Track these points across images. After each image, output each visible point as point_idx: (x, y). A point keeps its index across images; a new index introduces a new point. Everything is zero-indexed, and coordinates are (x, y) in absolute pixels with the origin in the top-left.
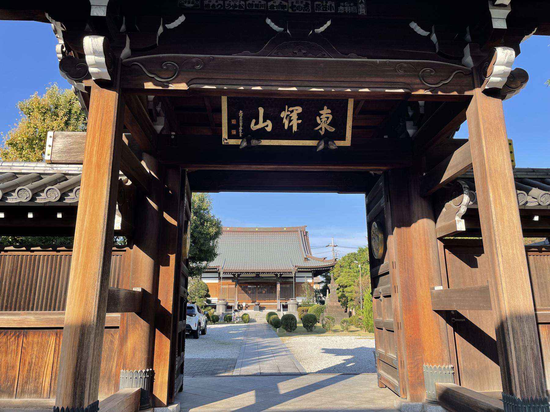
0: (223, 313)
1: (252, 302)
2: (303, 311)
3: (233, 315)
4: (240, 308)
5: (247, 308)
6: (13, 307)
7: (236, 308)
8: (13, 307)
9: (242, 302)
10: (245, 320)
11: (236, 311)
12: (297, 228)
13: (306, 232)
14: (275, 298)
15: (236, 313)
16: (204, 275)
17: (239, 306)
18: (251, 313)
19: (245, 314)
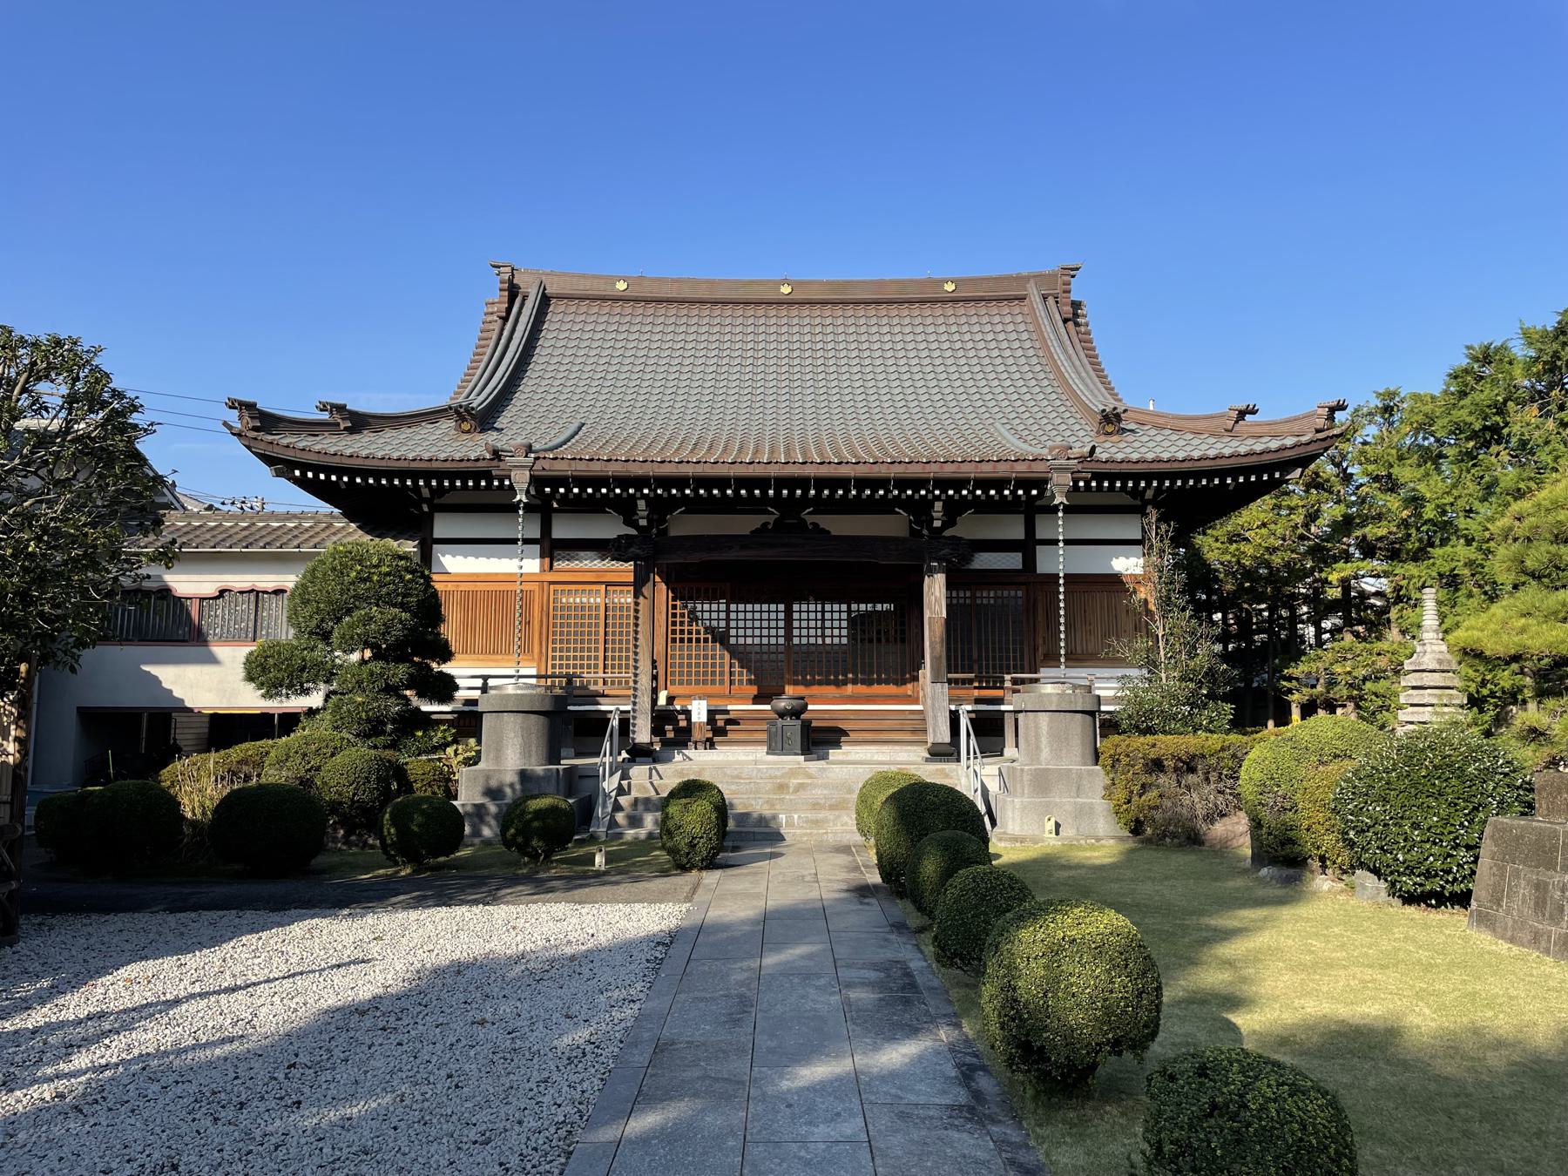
0: (524, 775)
1: (757, 700)
2: (1157, 765)
3: (610, 784)
4: (673, 730)
5: (720, 732)
6: (1026, 663)
7: (642, 733)
8: (1026, 663)
9: (690, 697)
10: (681, 841)
11: (640, 754)
12: (1022, 280)
13: (1076, 305)
14: (906, 671)
15: (639, 772)
16: (443, 526)
17: (662, 719)
18: (742, 769)
19: (691, 789)
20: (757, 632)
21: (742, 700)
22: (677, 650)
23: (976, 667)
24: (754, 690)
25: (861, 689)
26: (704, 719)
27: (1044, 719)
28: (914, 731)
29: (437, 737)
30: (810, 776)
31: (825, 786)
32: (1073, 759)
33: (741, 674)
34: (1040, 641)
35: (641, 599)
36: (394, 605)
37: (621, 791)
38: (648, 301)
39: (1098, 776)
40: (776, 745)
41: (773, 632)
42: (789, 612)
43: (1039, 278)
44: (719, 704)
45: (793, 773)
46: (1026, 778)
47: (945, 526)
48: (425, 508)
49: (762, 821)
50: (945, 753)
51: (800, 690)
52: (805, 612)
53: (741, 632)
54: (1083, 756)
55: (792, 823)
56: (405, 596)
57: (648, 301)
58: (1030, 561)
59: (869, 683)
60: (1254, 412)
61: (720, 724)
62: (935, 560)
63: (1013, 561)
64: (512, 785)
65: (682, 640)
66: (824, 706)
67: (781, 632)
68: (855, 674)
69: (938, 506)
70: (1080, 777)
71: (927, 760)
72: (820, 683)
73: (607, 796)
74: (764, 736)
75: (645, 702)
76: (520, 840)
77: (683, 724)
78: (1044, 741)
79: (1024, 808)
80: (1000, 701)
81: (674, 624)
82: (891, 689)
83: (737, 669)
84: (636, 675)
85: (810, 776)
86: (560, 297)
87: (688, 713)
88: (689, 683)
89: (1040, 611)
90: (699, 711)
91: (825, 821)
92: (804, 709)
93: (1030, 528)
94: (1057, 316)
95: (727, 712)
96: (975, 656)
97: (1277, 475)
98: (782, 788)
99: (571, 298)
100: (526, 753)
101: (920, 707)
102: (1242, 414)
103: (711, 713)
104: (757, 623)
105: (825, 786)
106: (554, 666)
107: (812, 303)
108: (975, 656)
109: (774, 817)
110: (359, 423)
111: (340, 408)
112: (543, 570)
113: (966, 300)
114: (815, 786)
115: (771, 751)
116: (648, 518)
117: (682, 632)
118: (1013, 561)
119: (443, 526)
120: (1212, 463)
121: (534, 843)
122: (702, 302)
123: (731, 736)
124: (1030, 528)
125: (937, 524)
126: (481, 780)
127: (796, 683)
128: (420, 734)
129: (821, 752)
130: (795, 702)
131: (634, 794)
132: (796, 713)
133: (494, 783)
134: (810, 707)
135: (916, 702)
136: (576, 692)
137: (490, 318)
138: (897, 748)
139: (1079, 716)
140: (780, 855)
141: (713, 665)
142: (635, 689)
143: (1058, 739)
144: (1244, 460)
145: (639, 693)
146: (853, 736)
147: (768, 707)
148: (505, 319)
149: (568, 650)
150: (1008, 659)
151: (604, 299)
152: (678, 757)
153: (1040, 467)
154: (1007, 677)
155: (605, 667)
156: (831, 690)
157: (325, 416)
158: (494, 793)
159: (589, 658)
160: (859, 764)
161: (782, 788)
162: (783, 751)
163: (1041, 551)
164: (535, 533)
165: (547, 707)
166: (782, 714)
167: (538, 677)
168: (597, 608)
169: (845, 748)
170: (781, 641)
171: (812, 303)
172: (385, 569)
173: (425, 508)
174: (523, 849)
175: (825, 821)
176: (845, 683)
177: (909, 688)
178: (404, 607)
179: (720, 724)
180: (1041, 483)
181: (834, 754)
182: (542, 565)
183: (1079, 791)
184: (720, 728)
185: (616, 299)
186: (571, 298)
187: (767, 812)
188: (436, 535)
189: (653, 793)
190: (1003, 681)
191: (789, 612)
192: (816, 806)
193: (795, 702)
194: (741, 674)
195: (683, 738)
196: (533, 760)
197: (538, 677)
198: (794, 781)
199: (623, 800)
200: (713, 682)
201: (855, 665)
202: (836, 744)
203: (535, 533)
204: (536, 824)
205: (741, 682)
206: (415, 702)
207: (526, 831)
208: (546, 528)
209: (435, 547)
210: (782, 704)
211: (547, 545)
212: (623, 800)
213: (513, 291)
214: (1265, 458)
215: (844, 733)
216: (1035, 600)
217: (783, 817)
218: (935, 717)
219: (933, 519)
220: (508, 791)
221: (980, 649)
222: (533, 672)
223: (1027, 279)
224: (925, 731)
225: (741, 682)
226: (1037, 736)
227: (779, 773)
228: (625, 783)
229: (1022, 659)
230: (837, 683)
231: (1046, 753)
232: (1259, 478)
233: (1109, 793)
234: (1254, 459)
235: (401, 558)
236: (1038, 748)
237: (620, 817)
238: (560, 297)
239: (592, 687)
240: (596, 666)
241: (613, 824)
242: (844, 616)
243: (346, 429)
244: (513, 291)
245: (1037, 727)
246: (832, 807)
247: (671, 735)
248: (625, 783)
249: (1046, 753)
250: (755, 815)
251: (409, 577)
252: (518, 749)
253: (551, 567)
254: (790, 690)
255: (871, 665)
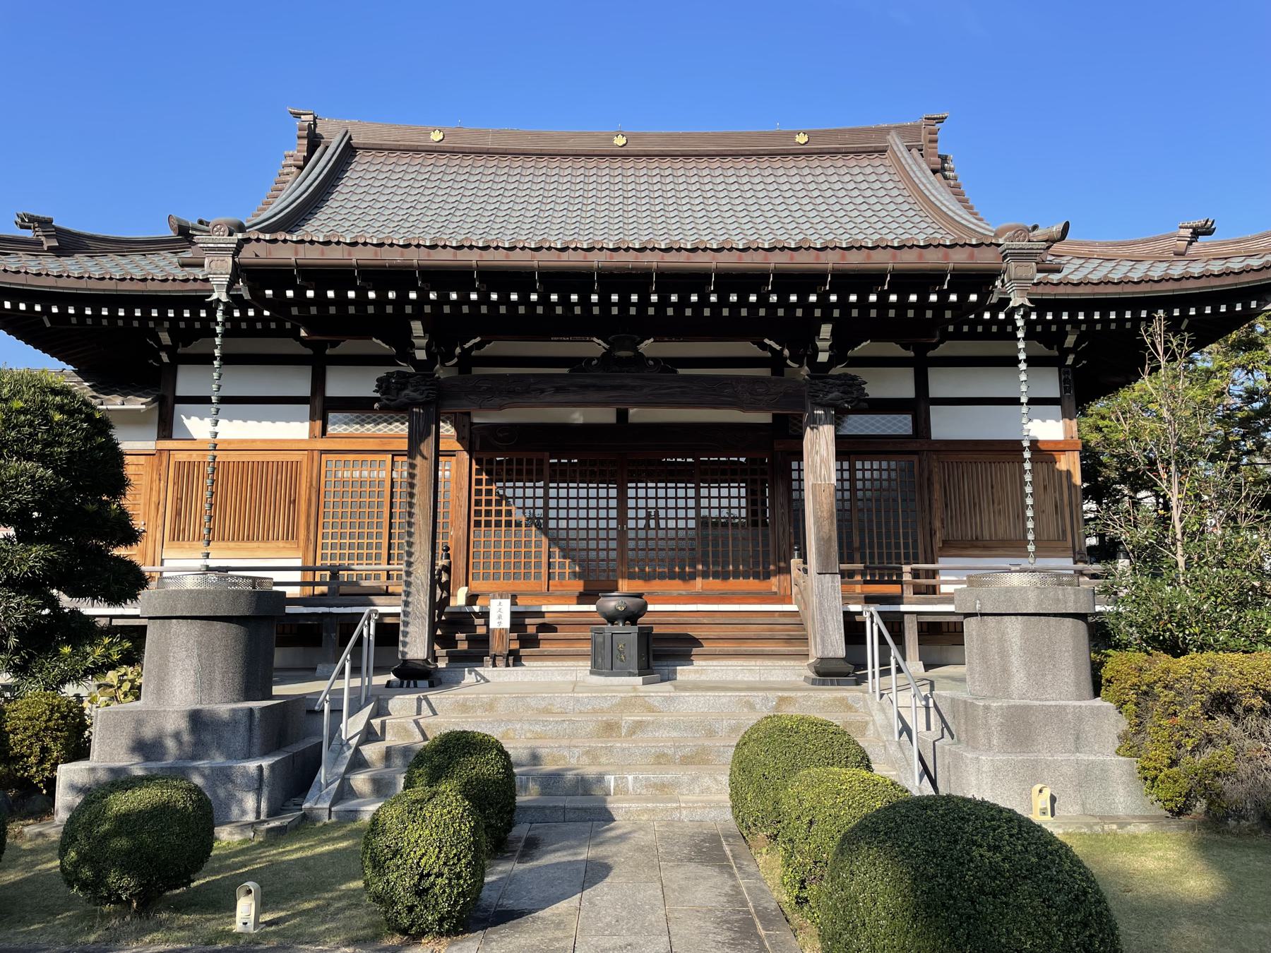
0: (196, 719)
1: (584, 598)
2: (1222, 703)
5: (529, 641)
7: (416, 646)
11: (415, 676)
13: (944, 159)
15: (402, 705)
18: (536, 706)
20: (583, 513)
21: (563, 599)
22: (479, 535)
23: (857, 556)
24: (579, 586)
25: (715, 584)
26: (506, 624)
27: (1014, 627)
28: (789, 640)
29: (96, 653)
30: (651, 710)
31: (674, 726)
32: (1064, 687)
33: (562, 566)
34: (937, 524)
35: (418, 460)
36: (29, 457)
37: (369, 735)
38: (466, 153)
39: (1107, 719)
40: (604, 663)
41: (603, 513)
42: (622, 498)
43: (901, 131)
44: (524, 604)
45: (626, 705)
46: (995, 721)
47: (832, 362)
48: (165, 358)
49: (584, 785)
50: (845, 671)
51: (638, 586)
52: (643, 495)
53: (563, 513)
54: (1077, 685)
55: (629, 801)
56: (47, 444)
57: (466, 153)
58: (922, 425)
59: (725, 576)
60: (1209, 232)
61: (531, 630)
62: (821, 406)
63: (901, 425)
64: (177, 736)
65: (498, 524)
66: (669, 606)
67: (613, 513)
68: (705, 563)
69: (826, 330)
70: (1080, 719)
71: (814, 682)
72: (662, 577)
73: (344, 744)
74: (587, 648)
75: (421, 602)
76: (86, 873)
77: (481, 631)
78: (1016, 662)
79: (997, 770)
80: (898, 600)
81: (478, 503)
82: (752, 584)
83: (557, 559)
84: (409, 564)
85: (651, 710)
86: (368, 149)
87: (485, 615)
88: (496, 577)
89: (937, 486)
90: (500, 614)
91: (675, 784)
92: (643, 610)
93: (921, 383)
94: (924, 166)
95: (541, 614)
96: (856, 544)
97: (1254, 305)
98: (610, 728)
99: (380, 149)
100: (204, 684)
101: (794, 608)
102: (1197, 233)
103: (518, 619)
104: (584, 505)
105: (674, 726)
106: (323, 557)
107: (649, 156)
108: (856, 544)
109: (600, 779)
110: (69, 244)
111: (45, 223)
112: (312, 436)
113: (821, 153)
114: (660, 726)
115: (596, 670)
116: (428, 348)
117: (488, 513)
118: (901, 425)
119: (188, 381)
120: (1176, 286)
121: (112, 878)
122: (527, 154)
123: (544, 647)
124: (921, 383)
125: (823, 357)
126: (128, 728)
127: (631, 576)
128: (67, 650)
129: (666, 670)
130: (629, 601)
131: (391, 740)
132: (631, 617)
133: (148, 733)
134: (650, 608)
135: (786, 599)
136: (343, 589)
137: (287, 170)
138: (768, 663)
139: (1069, 622)
140: (595, 873)
141: (527, 555)
142: (408, 584)
143: (1039, 658)
144: (1217, 282)
145: (413, 590)
146: (708, 647)
147: (593, 608)
148: (301, 168)
149: (360, 536)
150: (897, 546)
151: (417, 150)
152: (469, 678)
153: (986, 259)
154: (906, 568)
155: (389, 559)
156: (676, 586)
157: (29, 234)
158: (146, 748)
159: (369, 546)
160: (727, 692)
161: (610, 728)
162: (612, 671)
163: (936, 413)
164: (305, 391)
165: (242, 610)
166: (612, 618)
167: (302, 569)
168: (381, 483)
169: (698, 663)
170: (613, 524)
171: (649, 156)
172: (17, 404)
173: (165, 358)
174: (95, 887)
175: (675, 784)
176: (692, 576)
177: (774, 583)
178: (43, 459)
179: (531, 630)
180: (983, 280)
181: (684, 673)
182: (312, 430)
183: (1078, 742)
184: (529, 635)
185: (430, 151)
186: (380, 149)
187: (591, 771)
188: (181, 391)
189: (419, 737)
190: (900, 575)
191: (622, 498)
192: (661, 759)
193: (631, 602)
194: (562, 566)
195: (479, 650)
196: (217, 692)
197: (302, 569)
198: (629, 719)
199: (371, 752)
200: (527, 576)
201: (705, 554)
202: (686, 658)
203: (305, 391)
204: (122, 843)
205: (562, 575)
206: (66, 602)
207: (96, 858)
208: (319, 382)
209: (177, 406)
210: (612, 603)
211: (318, 403)
212: (371, 752)
213: (314, 141)
214: (1245, 278)
215: (695, 642)
216: (930, 472)
217: (611, 780)
218: (824, 621)
219: (816, 351)
220: (170, 744)
221: (862, 531)
222: (298, 563)
223: (887, 130)
224: (804, 640)
225: (562, 575)
226: (1004, 654)
227: (606, 705)
228: (376, 722)
229: (915, 547)
230: (684, 577)
231: (1019, 679)
232: (1231, 308)
233: (1130, 745)
234: (1230, 280)
235: (55, 392)
236: (1005, 670)
237: (360, 781)
238: (368, 149)
239: (365, 583)
240: (378, 556)
241: (345, 792)
242: (692, 513)
243: (51, 249)
244: (314, 141)
245: (1002, 639)
246: (687, 761)
247: (463, 646)
248: (376, 722)
249: (1019, 679)
250: (570, 775)
251: (58, 417)
252: (191, 676)
253: (324, 432)
254: (624, 586)
255: (726, 554)
